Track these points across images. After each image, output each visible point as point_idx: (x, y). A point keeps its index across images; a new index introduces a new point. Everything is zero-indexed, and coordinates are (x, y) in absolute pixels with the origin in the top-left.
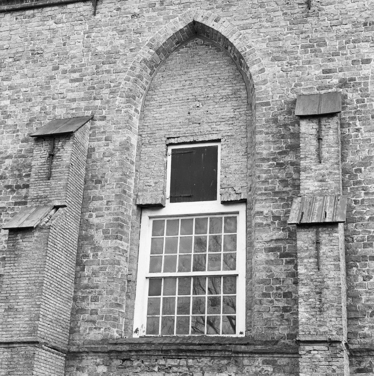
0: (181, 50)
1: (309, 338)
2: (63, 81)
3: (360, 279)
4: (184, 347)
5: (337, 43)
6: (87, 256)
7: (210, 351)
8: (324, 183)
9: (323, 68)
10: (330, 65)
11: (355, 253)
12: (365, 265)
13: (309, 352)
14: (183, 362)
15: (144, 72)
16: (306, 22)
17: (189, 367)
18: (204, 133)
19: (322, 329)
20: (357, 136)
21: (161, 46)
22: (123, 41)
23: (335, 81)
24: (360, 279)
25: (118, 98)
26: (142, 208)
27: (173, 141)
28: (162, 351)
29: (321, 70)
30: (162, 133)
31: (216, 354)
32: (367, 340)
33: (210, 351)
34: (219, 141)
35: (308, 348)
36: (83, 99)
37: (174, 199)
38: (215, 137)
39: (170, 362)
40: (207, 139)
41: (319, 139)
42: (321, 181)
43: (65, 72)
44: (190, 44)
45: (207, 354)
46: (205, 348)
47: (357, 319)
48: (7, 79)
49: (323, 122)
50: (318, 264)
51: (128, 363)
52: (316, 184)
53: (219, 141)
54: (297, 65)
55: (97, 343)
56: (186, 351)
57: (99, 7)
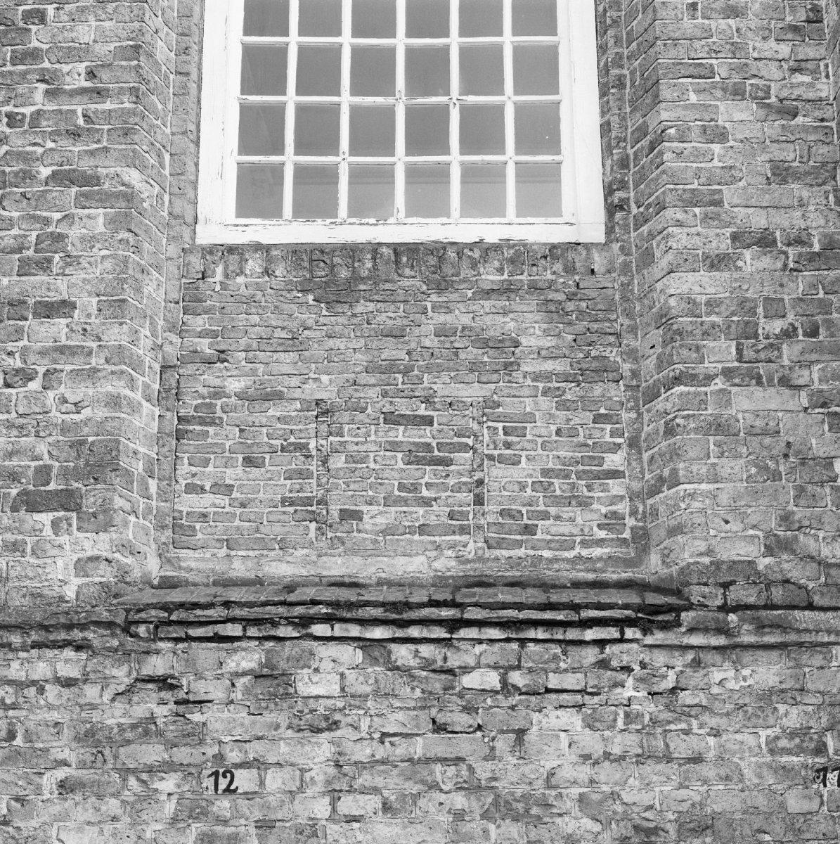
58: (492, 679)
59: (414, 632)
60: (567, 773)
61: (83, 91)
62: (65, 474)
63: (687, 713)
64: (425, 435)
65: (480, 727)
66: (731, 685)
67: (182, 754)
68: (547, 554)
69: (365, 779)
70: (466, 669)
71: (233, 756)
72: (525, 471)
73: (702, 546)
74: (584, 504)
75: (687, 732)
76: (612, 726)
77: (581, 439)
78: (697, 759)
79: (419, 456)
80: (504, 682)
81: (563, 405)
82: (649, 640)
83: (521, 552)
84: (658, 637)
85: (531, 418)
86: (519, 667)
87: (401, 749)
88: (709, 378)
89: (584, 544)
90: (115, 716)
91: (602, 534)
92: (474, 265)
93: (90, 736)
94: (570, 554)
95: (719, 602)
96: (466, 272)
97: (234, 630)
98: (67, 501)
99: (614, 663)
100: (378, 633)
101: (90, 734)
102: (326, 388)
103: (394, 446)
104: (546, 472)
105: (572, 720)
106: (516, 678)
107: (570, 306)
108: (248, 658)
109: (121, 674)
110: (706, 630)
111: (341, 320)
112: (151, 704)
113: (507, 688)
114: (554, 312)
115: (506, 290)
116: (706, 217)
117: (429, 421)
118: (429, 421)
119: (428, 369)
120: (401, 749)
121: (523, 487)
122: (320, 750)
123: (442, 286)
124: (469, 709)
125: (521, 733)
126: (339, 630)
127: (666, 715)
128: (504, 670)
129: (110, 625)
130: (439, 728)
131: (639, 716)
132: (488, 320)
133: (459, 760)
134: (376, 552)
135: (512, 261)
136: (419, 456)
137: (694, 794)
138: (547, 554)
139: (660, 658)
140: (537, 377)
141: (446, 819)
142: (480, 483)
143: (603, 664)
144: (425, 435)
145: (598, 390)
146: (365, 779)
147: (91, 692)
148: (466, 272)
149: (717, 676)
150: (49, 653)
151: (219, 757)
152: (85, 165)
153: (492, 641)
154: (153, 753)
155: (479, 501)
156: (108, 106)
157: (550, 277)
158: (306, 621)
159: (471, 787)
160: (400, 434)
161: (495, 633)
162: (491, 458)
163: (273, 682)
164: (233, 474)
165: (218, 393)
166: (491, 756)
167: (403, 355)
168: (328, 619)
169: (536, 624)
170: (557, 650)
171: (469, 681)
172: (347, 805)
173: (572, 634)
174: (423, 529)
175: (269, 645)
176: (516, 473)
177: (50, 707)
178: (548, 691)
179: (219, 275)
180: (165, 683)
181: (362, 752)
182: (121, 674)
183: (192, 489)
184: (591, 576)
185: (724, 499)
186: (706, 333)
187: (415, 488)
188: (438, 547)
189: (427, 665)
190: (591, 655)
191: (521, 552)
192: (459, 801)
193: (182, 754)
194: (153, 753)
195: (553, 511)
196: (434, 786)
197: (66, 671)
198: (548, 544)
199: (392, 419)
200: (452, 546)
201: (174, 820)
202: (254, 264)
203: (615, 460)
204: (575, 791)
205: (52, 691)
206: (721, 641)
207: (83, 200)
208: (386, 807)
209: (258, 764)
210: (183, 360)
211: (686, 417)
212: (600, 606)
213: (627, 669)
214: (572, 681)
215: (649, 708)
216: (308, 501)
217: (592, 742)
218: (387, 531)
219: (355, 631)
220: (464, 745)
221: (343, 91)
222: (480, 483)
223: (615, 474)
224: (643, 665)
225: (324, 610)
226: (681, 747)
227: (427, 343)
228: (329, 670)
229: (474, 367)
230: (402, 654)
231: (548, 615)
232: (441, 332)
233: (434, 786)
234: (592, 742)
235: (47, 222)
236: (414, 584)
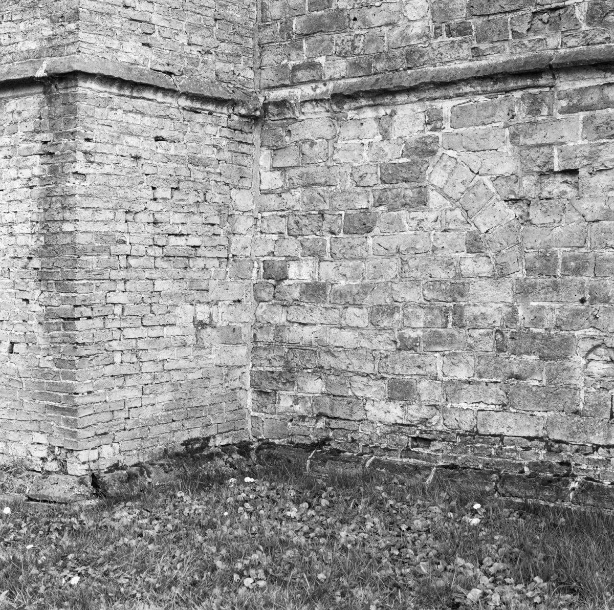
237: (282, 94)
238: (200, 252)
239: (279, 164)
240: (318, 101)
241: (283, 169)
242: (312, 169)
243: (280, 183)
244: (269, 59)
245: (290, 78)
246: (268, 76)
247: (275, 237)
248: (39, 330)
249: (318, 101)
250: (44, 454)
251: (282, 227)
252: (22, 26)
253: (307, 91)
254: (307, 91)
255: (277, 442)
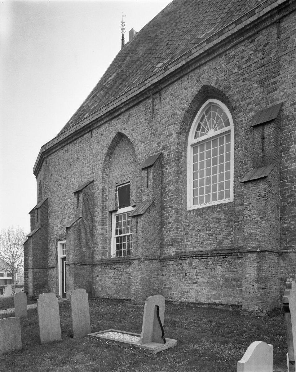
0: (118, 145)
1: (133, 258)
2: (85, 168)
3: (165, 232)
4: (118, 261)
5: (162, 129)
6: (95, 232)
7: (124, 262)
8: (148, 196)
9: (157, 142)
10: (159, 140)
11: (164, 222)
12: (166, 227)
13: (133, 263)
14: (118, 266)
15: (106, 158)
16: (152, 121)
17: (120, 268)
18: (126, 179)
19: (137, 255)
20: (166, 172)
21: (110, 146)
22: (99, 147)
23: (161, 147)
24: (165, 232)
25: (99, 171)
26: (111, 212)
27: (117, 185)
28: (113, 263)
29: (156, 144)
30: (114, 182)
31: (126, 263)
32: (166, 255)
33: (124, 262)
34: (129, 182)
35: (133, 261)
36: (91, 174)
37: (120, 207)
38: (128, 181)
39: (115, 266)
40: (126, 182)
41: (148, 178)
42: (147, 196)
43: (86, 164)
44: (121, 142)
45: (124, 263)
46: (123, 261)
47: (163, 247)
48: (72, 171)
49: (149, 169)
50: (137, 230)
51: (106, 267)
52: (146, 197)
53: (129, 182)
54: (149, 144)
55: (98, 261)
56: (122, 262)
57: (93, 133)
58: (212, 263)
59: (203, 258)
60: (219, 273)
61: (171, 196)
62: (171, 242)
63: (233, 266)
64: (211, 232)
65: (210, 268)
66: (238, 262)
67: (182, 272)
68: (224, 246)
69: (199, 274)
70: (209, 262)
71: (187, 272)
72: (221, 235)
73: (237, 245)
74: (228, 239)
75: (233, 268)
76: (224, 268)
77: (228, 230)
78: (234, 272)
79: (210, 235)
80: (213, 263)
81: (226, 226)
82: (229, 257)
83: (221, 246)
84: (230, 257)
85: (222, 228)
86: (214, 261)
87: (203, 271)
88: (239, 222)
89: (228, 244)
90: (176, 268)
91: (230, 243)
92: (216, 208)
93: (174, 270)
94: (226, 246)
95: (238, 252)
96: (215, 209)
97: (186, 258)
98: (171, 245)
99: (225, 260)
100: (200, 258)
101: (175, 270)
102: (200, 227)
103: (207, 234)
104: (224, 235)
105: (220, 267)
106: (214, 262)
107: (227, 212)
108: (188, 261)
109: (177, 263)
110: (235, 256)
111: (201, 218)
112: (180, 267)
113: (213, 264)
114: (225, 213)
115: (220, 211)
116: (240, 198)
117: (211, 230)
118: (211, 230)
119: (210, 223)
120: (203, 271)
121: (221, 237)
122: (195, 271)
123: (212, 212)
124: (209, 266)
125: (215, 269)
126: (196, 258)
127: (231, 266)
128: (213, 261)
129: (175, 258)
130: (206, 268)
131: (227, 266)
132: (218, 216)
133: (208, 272)
134: (205, 247)
135: (221, 207)
136: (210, 235)
137: (233, 276)
138: (224, 246)
139: (230, 259)
140: (223, 223)
141: (207, 278)
142: (216, 237)
143: (224, 260)
144: (211, 232)
145: (230, 223)
146: (199, 274)
147: (174, 265)
148: (215, 209)
149: (237, 261)
150: (171, 261)
151: (186, 272)
152: (172, 205)
153: (212, 258)
154: (180, 272)
155: (216, 240)
156: (174, 197)
157: (225, 208)
158: (193, 257)
159: (210, 275)
160: (208, 232)
161: (212, 257)
162: (218, 234)
163: (190, 264)
164: (190, 239)
165: (189, 229)
166: (212, 271)
167: (208, 222)
168: (195, 257)
169: (216, 256)
170: (219, 259)
171: (209, 263)
172: (198, 277)
173: (220, 257)
174: (210, 244)
175: (190, 260)
176: (220, 236)
177: (171, 267)
178: (218, 264)
179: (188, 215)
180: (181, 264)
181: (199, 271)
182: (177, 263)
183: (187, 241)
184: (229, 248)
185: (240, 238)
186: (239, 215)
187: (209, 239)
188: (212, 246)
189: (205, 261)
190: (222, 259)
191: (221, 246)
192: (208, 276)
193: (182, 272)
194: (180, 272)
195: (224, 240)
196: (206, 275)
197: (172, 263)
198: (224, 245)
199: (207, 230)
200: (213, 246)
201: (182, 278)
202: (192, 213)
203: (232, 233)
204: (220, 275)
205: (171, 265)
206: (237, 257)
207: (172, 209)
208: (201, 277)
209: (189, 273)
210: (185, 226)
211: (236, 228)
212: (223, 253)
213: (226, 261)
214: (220, 263)
215: (229, 266)
216: (198, 242)
217: (222, 269)
218: (206, 244)
219: (198, 258)
220: (209, 270)
221: (231, 169)
222: (216, 237)
223: (232, 235)
224: (228, 260)
225: (194, 255)
226: (232, 270)
227: (210, 220)
228: (195, 262)
229: (216, 222)
230: (203, 260)
231: (212, 255)
232: (213, 218)
233: (206, 275)
234: (222, 269)
235: (168, 213)
236: (208, 251)
237: (286, 251)
238: (276, 277)
239: (285, 262)
240: (293, 252)
241: (286, 263)
242: (292, 263)
243: (285, 265)
244: (282, 245)
245: (288, 248)
246: (282, 248)
247: (284, 274)
248: (256, 290)
249: (293, 252)
250: (257, 309)
251: (286, 272)
252: (251, 243)
253: (291, 250)
254: (291, 250)
255: (151, 297)
